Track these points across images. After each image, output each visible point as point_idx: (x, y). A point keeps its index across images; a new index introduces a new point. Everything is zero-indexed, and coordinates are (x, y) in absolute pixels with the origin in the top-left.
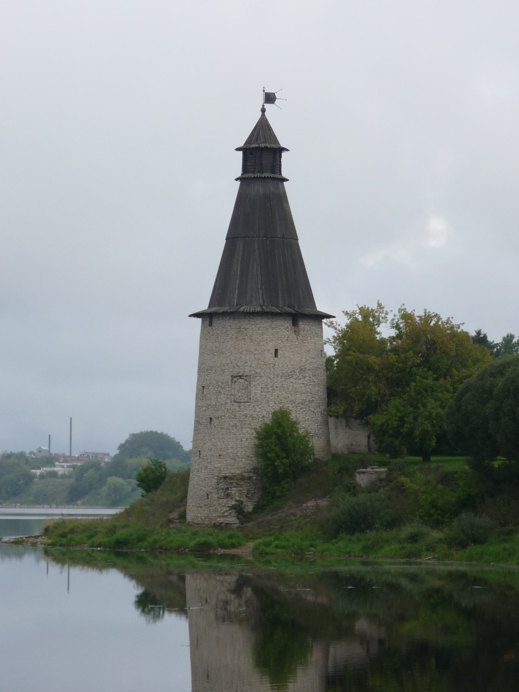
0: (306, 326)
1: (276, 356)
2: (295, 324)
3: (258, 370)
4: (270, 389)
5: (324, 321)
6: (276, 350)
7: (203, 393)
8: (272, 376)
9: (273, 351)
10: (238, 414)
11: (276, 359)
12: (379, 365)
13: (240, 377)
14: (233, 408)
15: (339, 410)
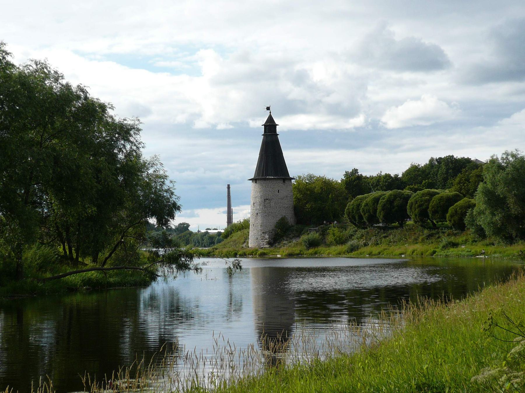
2: (284, 182)
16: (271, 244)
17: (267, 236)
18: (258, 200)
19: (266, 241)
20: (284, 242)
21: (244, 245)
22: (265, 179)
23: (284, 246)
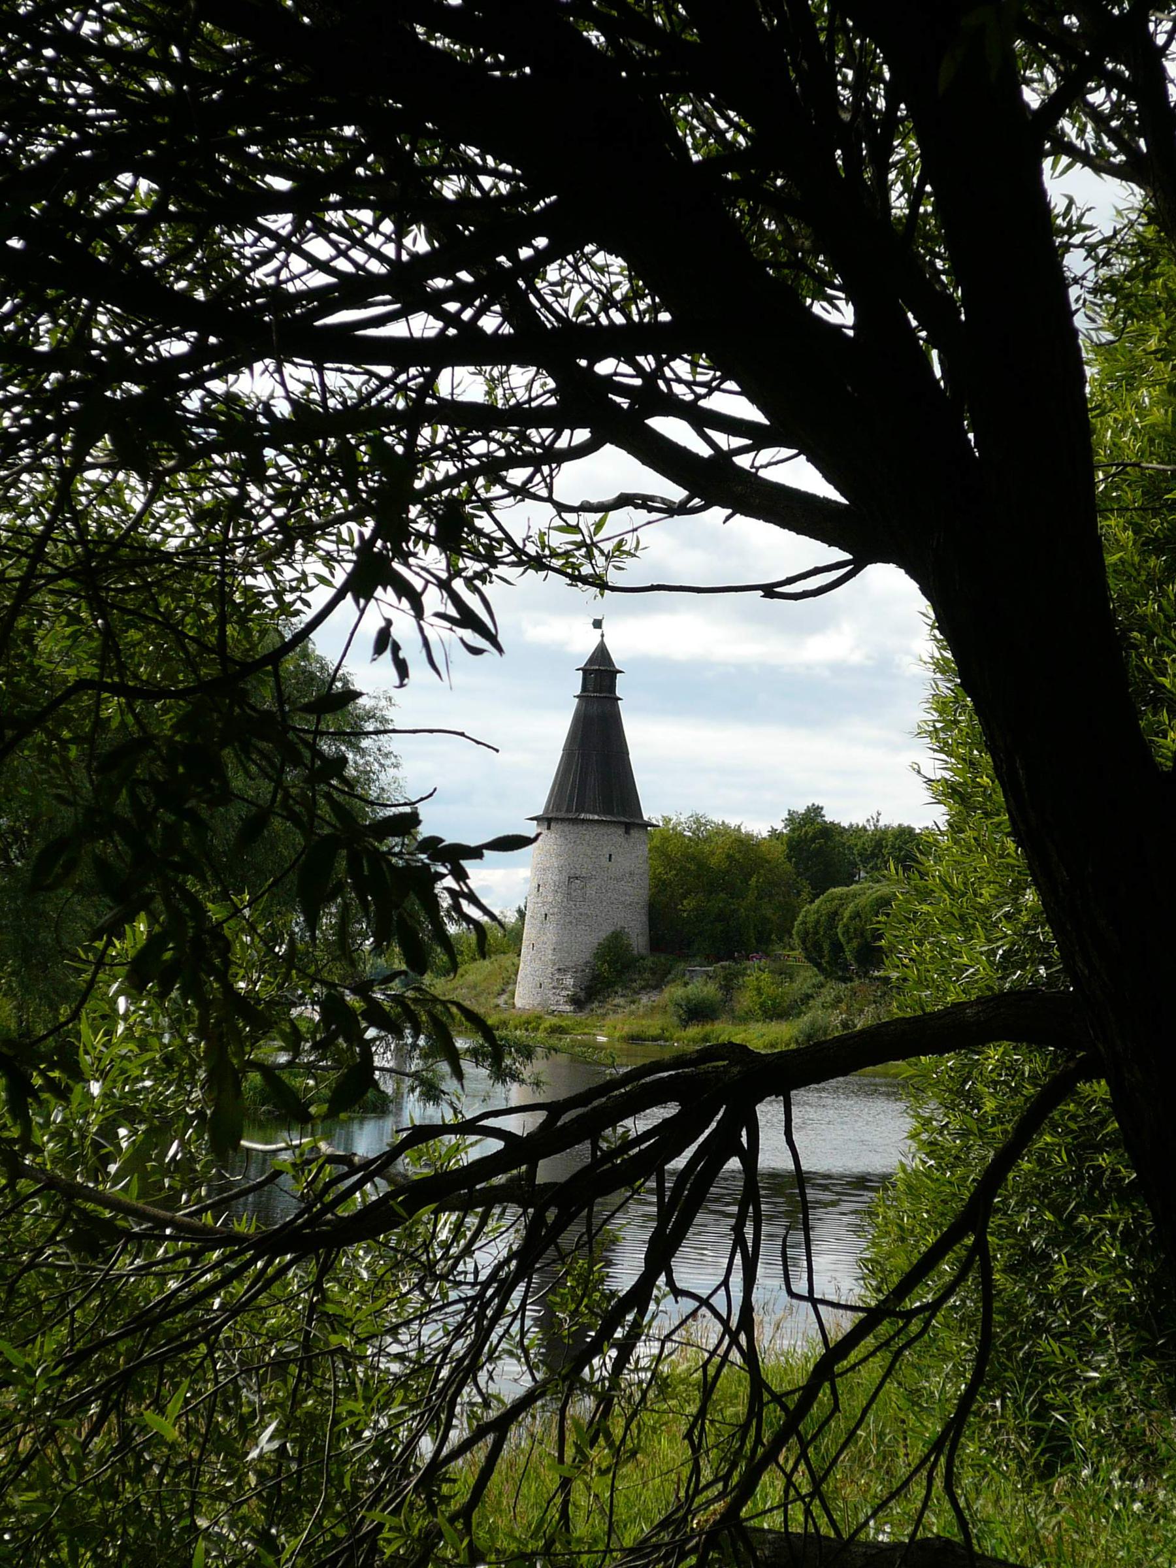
2: (627, 832)
16: (578, 1003)
17: (569, 981)
18: (552, 877)
19: (564, 993)
20: (616, 1001)
22: (575, 821)
23: (615, 1012)
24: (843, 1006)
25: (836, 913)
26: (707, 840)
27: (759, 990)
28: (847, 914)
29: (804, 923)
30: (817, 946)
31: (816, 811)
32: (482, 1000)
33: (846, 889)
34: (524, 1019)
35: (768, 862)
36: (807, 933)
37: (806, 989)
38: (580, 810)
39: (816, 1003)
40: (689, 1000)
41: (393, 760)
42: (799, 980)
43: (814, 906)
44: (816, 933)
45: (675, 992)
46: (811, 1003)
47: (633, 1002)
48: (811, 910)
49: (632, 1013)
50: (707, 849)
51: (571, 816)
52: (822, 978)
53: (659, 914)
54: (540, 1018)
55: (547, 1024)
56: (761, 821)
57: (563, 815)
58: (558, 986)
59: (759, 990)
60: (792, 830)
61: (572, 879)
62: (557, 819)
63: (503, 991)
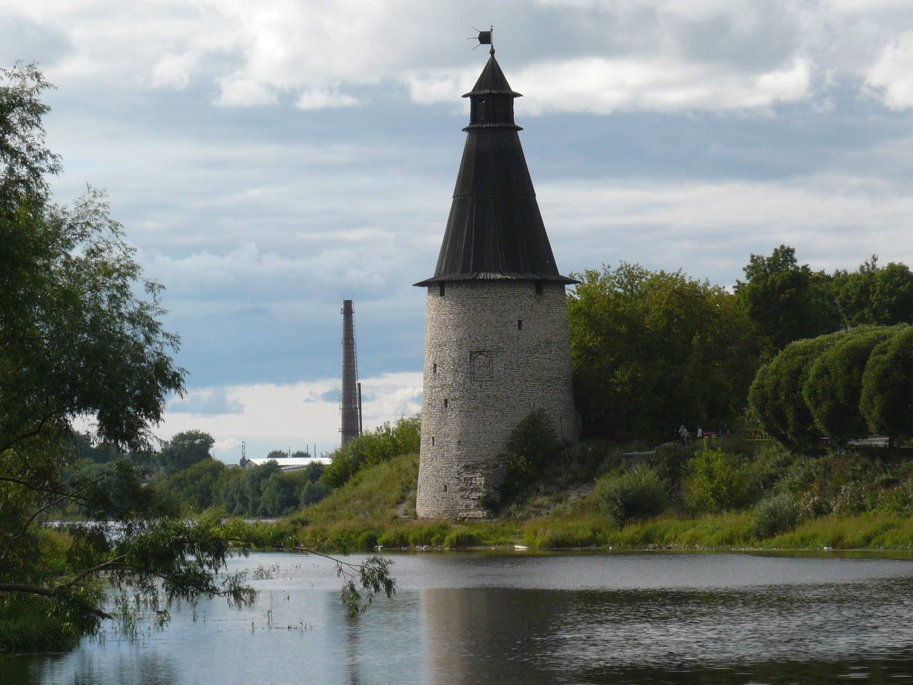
0: (551, 295)
1: (520, 328)
2: (539, 291)
3: (500, 345)
4: (514, 366)
5: (567, 286)
6: (520, 322)
7: (435, 372)
8: (516, 351)
9: (517, 323)
10: (479, 395)
11: (520, 331)
12: (538, 490)
13: (480, 353)
14: (473, 387)
15: (71, 467)
16: (492, 506)
17: (479, 480)
18: (450, 354)
19: (475, 495)
20: (539, 501)
21: (400, 511)
22: (474, 283)
23: (538, 514)
24: (815, 486)
25: (799, 372)
26: (643, 295)
27: (710, 474)
28: (812, 371)
29: (760, 386)
30: (779, 415)
31: (786, 254)
32: (378, 512)
33: (812, 341)
34: (424, 531)
35: (716, 316)
36: (765, 399)
37: (769, 467)
38: (479, 268)
39: (784, 483)
40: (624, 493)
41: (51, 161)
42: (761, 457)
43: (773, 365)
44: (777, 398)
45: (608, 484)
46: (777, 485)
47: (560, 501)
48: (770, 368)
49: (557, 514)
50: (641, 305)
51: (468, 276)
52: (788, 454)
53: (585, 389)
54: (444, 527)
55: (452, 535)
56: (723, 273)
57: (458, 276)
58: (467, 488)
59: (710, 474)
60: (756, 280)
61: (474, 354)
62: (450, 283)
63: (403, 499)
